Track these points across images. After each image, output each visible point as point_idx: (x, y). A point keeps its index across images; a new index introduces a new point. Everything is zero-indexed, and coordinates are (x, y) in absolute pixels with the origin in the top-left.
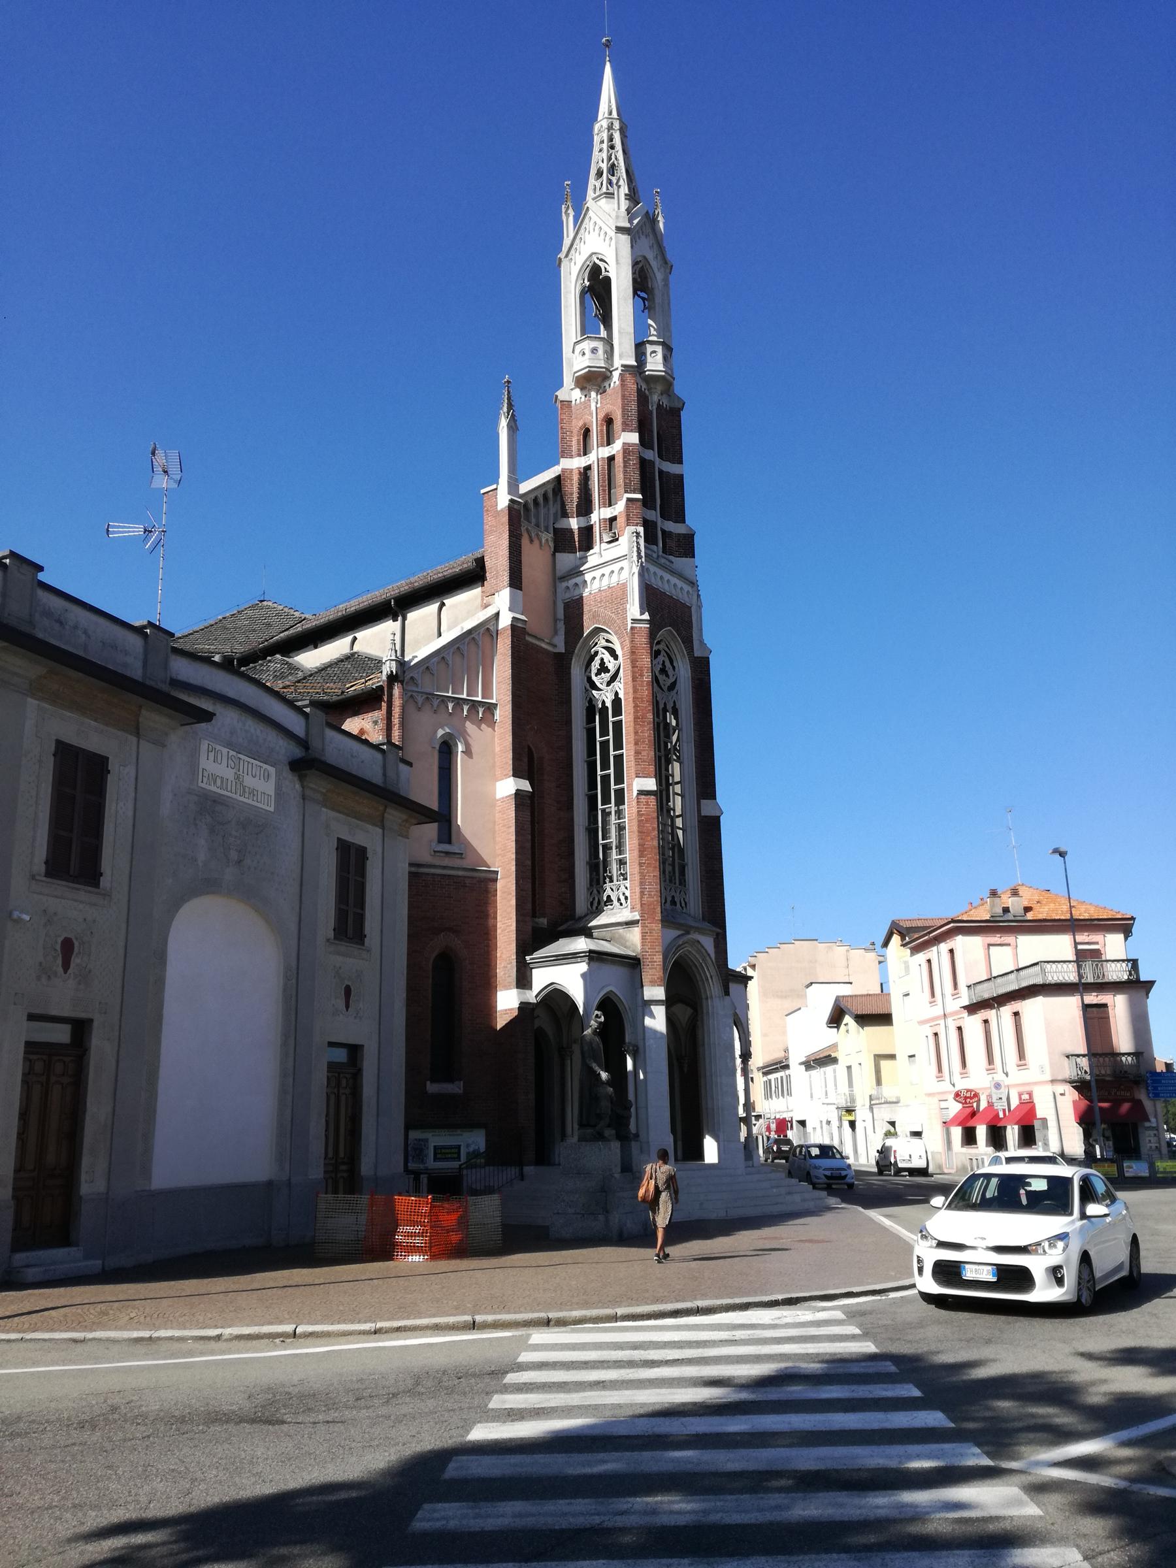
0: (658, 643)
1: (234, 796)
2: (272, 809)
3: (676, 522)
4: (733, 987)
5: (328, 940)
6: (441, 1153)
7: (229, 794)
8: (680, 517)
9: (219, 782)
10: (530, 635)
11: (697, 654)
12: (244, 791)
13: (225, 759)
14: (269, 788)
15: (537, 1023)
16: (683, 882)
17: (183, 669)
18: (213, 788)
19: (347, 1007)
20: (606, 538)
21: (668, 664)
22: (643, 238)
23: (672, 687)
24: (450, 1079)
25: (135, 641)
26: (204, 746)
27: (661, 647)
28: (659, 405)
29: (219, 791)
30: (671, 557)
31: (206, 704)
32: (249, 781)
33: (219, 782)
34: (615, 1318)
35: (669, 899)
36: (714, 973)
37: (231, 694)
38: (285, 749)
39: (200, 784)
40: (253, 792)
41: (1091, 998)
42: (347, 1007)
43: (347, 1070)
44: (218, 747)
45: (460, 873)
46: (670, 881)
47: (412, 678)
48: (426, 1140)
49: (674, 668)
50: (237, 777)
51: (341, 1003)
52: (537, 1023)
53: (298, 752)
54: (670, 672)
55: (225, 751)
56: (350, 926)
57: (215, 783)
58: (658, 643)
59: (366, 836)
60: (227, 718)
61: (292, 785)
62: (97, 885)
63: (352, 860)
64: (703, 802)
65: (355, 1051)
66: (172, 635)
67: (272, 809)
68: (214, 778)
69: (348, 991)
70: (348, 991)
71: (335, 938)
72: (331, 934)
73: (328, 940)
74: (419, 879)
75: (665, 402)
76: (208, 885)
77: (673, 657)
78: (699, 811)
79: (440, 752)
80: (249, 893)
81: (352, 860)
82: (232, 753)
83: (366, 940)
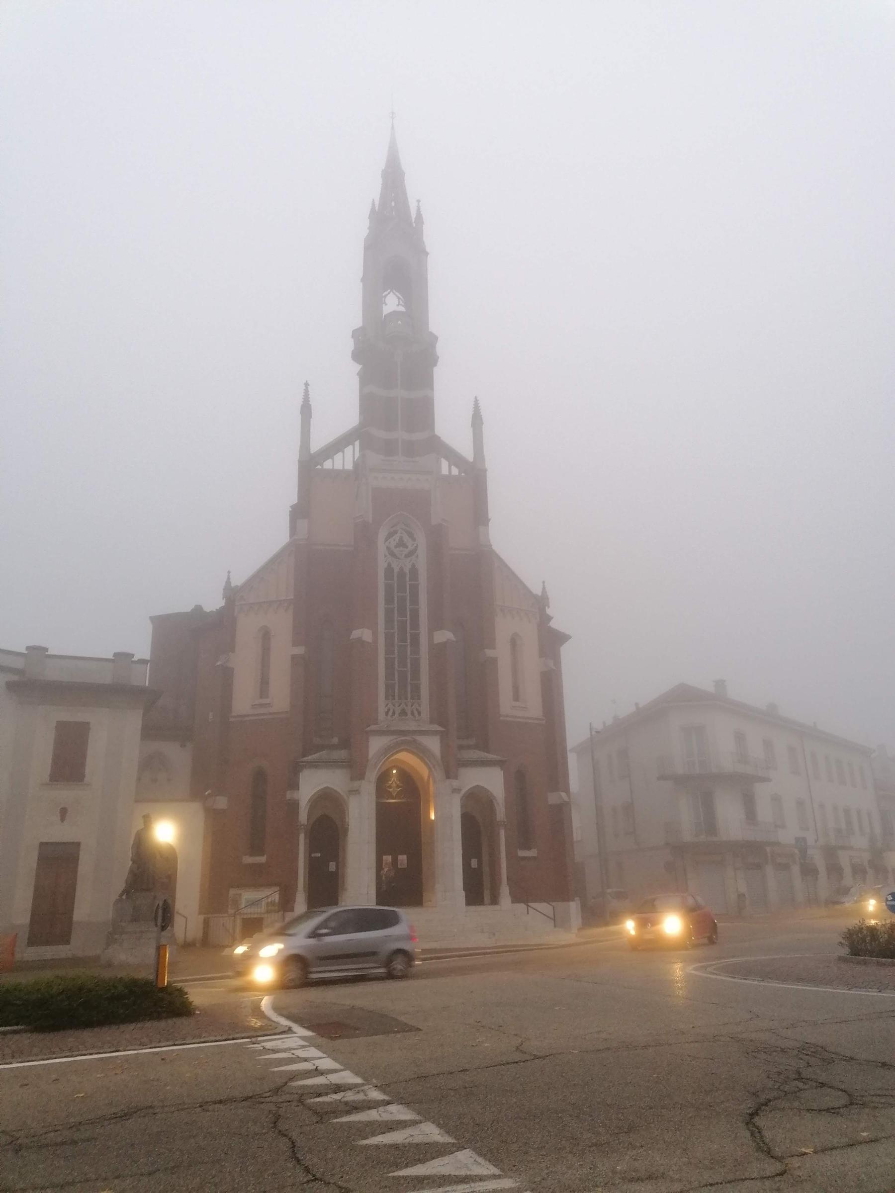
6: (254, 903)
24: (529, 848)
48: (240, 895)
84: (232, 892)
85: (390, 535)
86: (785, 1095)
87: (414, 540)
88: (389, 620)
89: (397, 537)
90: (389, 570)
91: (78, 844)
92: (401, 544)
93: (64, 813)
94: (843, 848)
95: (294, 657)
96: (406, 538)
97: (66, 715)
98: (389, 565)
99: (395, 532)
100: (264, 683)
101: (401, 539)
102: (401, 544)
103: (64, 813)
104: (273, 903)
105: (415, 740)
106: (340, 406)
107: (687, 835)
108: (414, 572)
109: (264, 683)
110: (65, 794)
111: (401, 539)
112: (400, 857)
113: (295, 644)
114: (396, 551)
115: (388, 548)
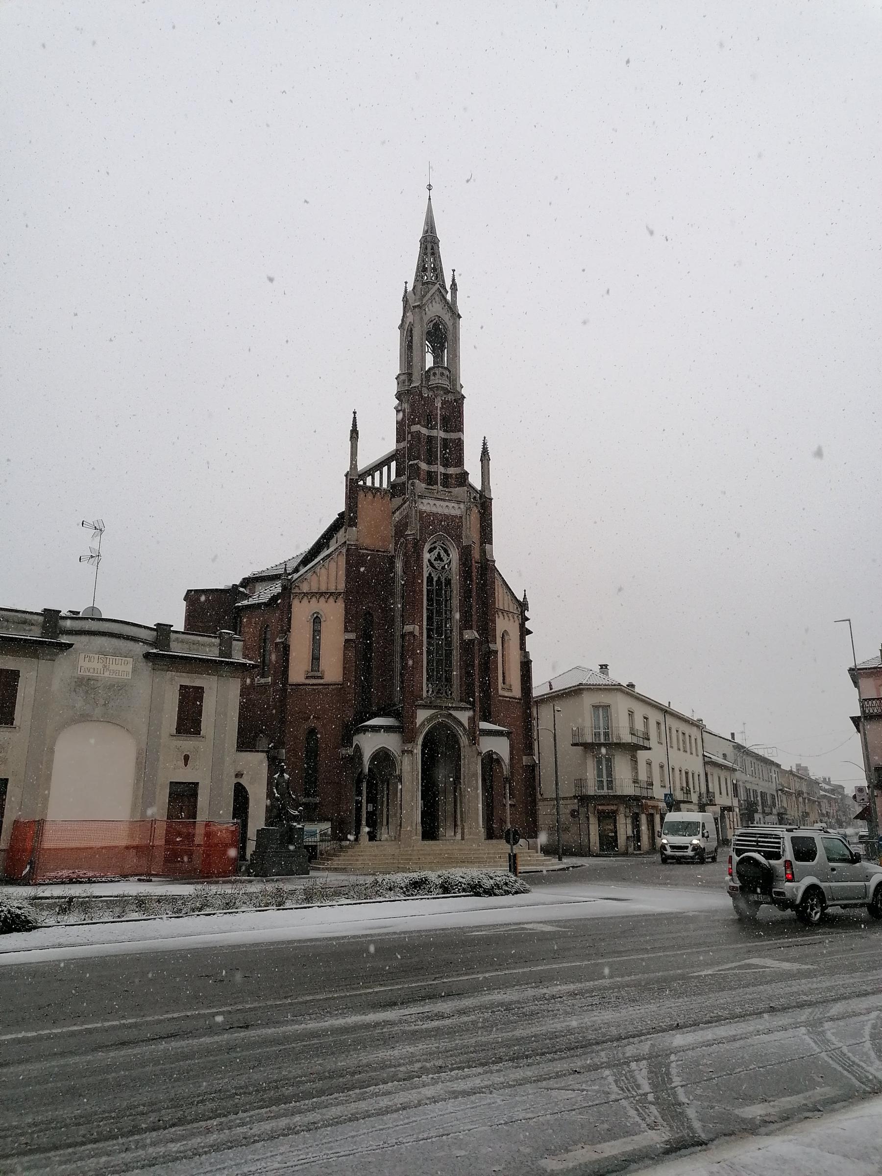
32: (113, 667)
61: (146, 668)
85: (430, 551)
86: (518, 981)
87: (448, 555)
88: (430, 619)
89: (436, 552)
90: (430, 579)
91: (196, 784)
92: (439, 558)
93: (186, 758)
94: (684, 802)
95: (347, 641)
96: (442, 553)
97: (187, 682)
98: (430, 574)
99: (435, 548)
100: (316, 659)
101: (439, 554)
102: (439, 558)
103: (186, 758)
104: (325, 834)
105: (451, 714)
106: (381, 440)
107: (591, 790)
109: (316, 659)
110: (188, 744)
111: (439, 554)
113: (346, 630)
114: (434, 563)
115: (429, 561)
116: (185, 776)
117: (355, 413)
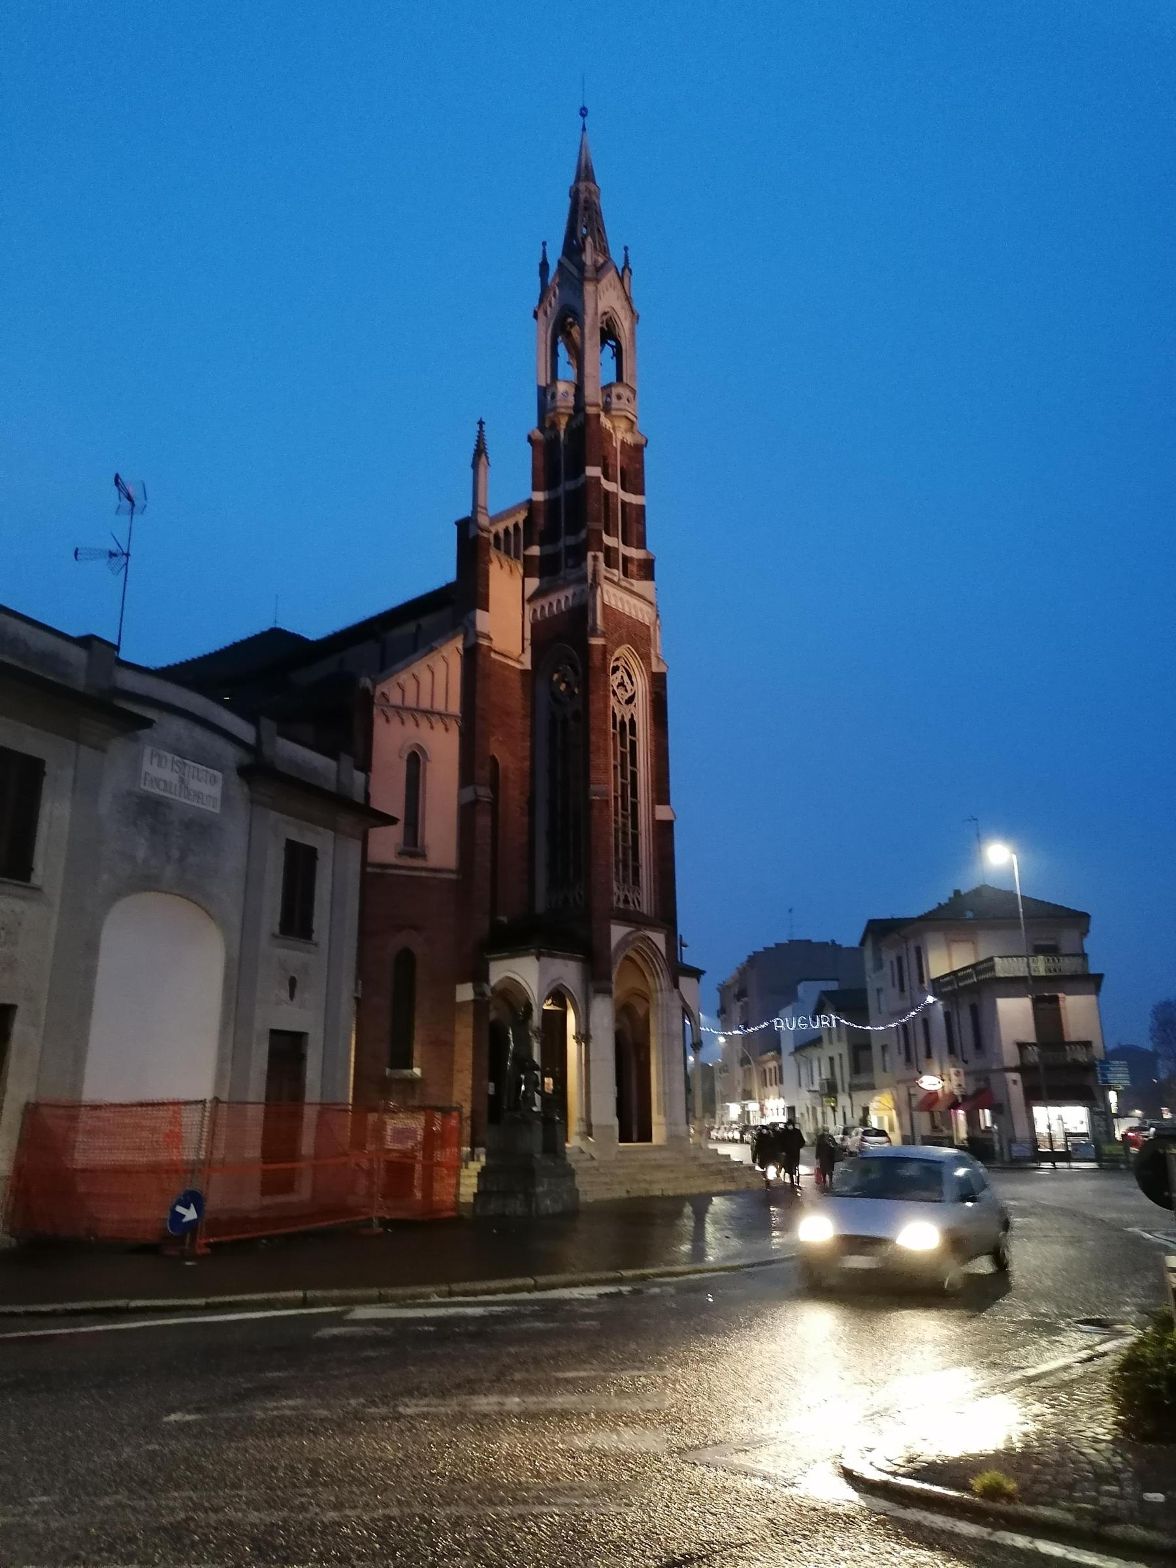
0: (617, 659)
1: (177, 798)
2: (217, 811)
3: (637, 548)
4: (683, 981)
5: (274, 935)
7: (173, 797)
8: (641, 544)
9: (162, 785)
10: (496, 652)
11: (655, 669)
12: (189, 794)
13: (169, 764)
14: (216, 791)
15: (493, 1015)
16: (636, 882)
17: (128, 681)
18: (156, 791)
19: (292, 996)
20: (570, 562)
21: (626, 679)
22: (611, 290)
23: (630, 700)
25: (78, 655)
26: (148, 751)
27: (618, 663)
28: (623, 443)
29: (162, 793)
30: (633, 581)
31: (150, 714)
32: (194, 785)
33: (162, 785)
34: (451, 1294)
35: (622, 898)
36: (664, 967)
37: (179, 703)
38: (232, 755)
39: (142, 786)
40: (198, 795)
41: (412, 849)
42: (292, 996)
43: (287, 1050)
44: (162, 752)
45: (424, 874)
46: (624, 881)
47: (383, 694)
49: (632, 683)
50: (182, 780)
51: (285, 994)
52: (493, 1015)
53: (247, 759)
54: (629, 686)
55: (169, 756)
56: (296, 921)
57: (158, 786)
58: (617, 659)
59: (319, 839)
60: (176, 727)
61: (239, 790)
62: (27, 878)
63: (300, 863)
64: (658, 807)
65: (298, 1039)
66: (388, 700)
67: (217, 811)
68: (156, 781)
69: (293, 983)
70: (293, 983)
71: (282, 932)
72: (277, 929)
73: (274, 935)
74: (373, 880)
75: (630, 439)
76: (147, 882)
77: (632, 672)
78: (653, 815)
79: (408, 761)
80: (192, 890)
81: (300, 863)
82: (177, 758)
83: (314, 935)
84: (372, 1117)
108: (632, 723)
112: (546, 1080)
116: (290, 1018)
117: (481, 423)
